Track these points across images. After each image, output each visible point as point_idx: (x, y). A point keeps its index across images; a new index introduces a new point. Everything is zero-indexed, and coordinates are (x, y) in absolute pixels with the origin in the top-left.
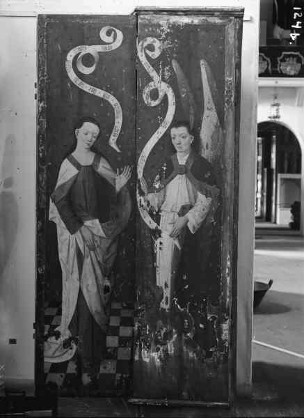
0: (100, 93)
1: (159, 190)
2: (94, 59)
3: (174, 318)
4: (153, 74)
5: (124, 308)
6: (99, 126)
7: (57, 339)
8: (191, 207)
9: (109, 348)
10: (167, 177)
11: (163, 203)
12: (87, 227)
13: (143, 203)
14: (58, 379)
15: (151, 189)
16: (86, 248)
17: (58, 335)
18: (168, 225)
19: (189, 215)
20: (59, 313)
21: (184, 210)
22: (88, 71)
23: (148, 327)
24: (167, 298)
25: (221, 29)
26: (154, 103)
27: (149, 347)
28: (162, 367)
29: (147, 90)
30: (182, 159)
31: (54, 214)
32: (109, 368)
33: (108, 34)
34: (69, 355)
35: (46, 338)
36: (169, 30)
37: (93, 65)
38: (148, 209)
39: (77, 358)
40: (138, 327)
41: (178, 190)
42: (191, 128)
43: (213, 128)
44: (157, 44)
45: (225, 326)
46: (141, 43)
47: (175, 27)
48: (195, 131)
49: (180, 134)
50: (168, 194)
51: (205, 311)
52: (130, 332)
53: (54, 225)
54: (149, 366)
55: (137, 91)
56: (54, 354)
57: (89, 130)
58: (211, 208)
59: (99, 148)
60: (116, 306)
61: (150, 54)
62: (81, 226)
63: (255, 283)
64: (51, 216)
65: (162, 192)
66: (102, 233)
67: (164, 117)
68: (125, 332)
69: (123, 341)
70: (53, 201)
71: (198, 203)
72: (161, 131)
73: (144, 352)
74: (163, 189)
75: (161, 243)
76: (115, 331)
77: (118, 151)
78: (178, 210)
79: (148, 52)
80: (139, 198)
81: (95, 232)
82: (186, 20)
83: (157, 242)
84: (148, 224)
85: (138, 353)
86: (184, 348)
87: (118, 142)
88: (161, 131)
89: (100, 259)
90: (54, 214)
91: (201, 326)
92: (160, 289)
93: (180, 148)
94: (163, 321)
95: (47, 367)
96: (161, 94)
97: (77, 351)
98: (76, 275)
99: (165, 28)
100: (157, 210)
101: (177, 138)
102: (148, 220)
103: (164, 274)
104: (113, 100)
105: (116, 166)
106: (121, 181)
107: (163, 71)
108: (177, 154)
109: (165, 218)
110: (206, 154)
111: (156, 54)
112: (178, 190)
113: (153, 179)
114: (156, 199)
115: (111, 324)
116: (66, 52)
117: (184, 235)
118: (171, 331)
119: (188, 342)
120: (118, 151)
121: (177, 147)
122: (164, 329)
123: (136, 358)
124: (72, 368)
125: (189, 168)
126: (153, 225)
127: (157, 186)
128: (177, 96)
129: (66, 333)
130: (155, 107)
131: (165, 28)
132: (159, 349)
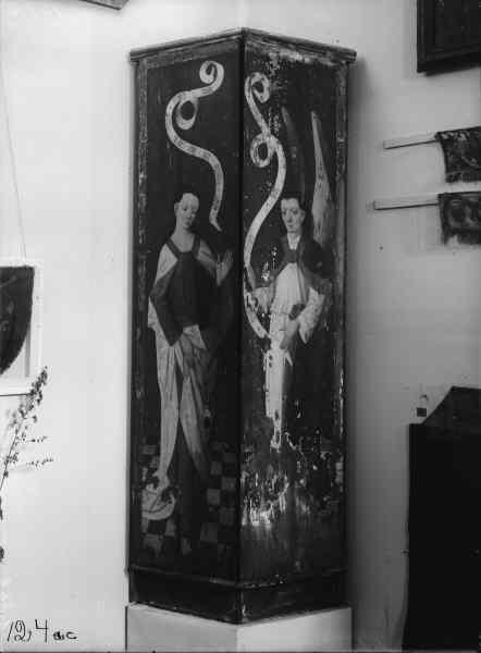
0: (200, 152)
1: (268, 284)
2: (193, 109)
3: (287, 460)
4: (262, 123)
5: (227, 451)
6: (199, 197)
7: (155, 487)
8: (303, 307)
9: (210, 505)
10: (278, 266)
11: (272, 301)
12: (186, 335)
13: (252, 302)
14: (154, 541)
15: (260, 283)
16: (187, 367)
17: (156, 482)
18: (278, 333)
19: (301, 318)
20: (158, 453)
21: (297, 310)
22: (186, 125)
23: (257, 476)
24: (278, 433)
25: (332, 72)
26: (264, 164)
27: (258, 505)
28: (274, 531)
29: (255, 145)
30: (293, 242)
31: (153, 319)
32: (209, 535)
33: (208, 72)
34: (166, 513)
35: (143, 485)
36: (278, 67)
37: (191, 118)
38: (256, 309)
39: (176, 516)
40: (246, 478)
41: (289, 283)
42: (302, 201)
43: (325, 203)
44: (266, 84)
45: (339, 466)
46: (248, 79)
47: (284, 62)
48: (306, 207)
49: (290, 204)
50: (278, 288)
51: (319, 447)
52: (232, 486)
53: (151, 333)
54: (258, 531)
55: (242, 146)
56: (152, 507)
57: (189, 200)
58: (323, 309)
59: (199, 227)
60: (217, 447)
61: (258, 95)
62: (179, 335)
63: (451, 180)
64: (150, 321)
65: (272, 285)
66: (202, 344)
67: (274, 184)
68: (228, 484)
69: (225, 497)
70: (153, 301)
71: (311, 301)
72: (270, 202)
73: (253, 512)
74: (272, 282)
75: (271, 358)
76: (217, 486)
77: (219, 229)
78: (290, 310)
79: (256, 92)
80: (246, 294)
81: (195, 342)
82: (297, 56)
83: (266, 356)
84: (256, 330)
85: (245, 515)
86: (297, 500)
87: (218, 219)
88: (270, 202)
89: (200, 377)
90: (153, 319)
91: (315, 468)
92: (270, 421)
93: (291, 226)
94: (273, 465)
95: (145, 524)
96: (270, 152)
97: (177, 504)
98: (174, 403)
99: (274, 63)
100: (266, 310)
101: (288, 212)
102: (256, 325)
103: (274, 403)
104: (213, 161)
105: (217, 252)
106: (222, 270)
107: (273, 121)
108: (289, 235)
109: (278, 321)
110: (318, 236)
111: (265, 96)
112: (289, 283)
113: (262, 267)
114: (265, 296)
115: (212, 472)
116: (165, 104)
117: (297, 347)
118: (283, 479)
119: (303, 493)
120: (219, 229)
121: (287, 225)
122: (275, 477)
123: (244, 523)
124: (170, 529)
125: (301, 253)
126: (261, 333)
127: (266, 278)
128: (286, 150)
129: (165, 483)
130: (264, 168)
131: (274, 63)
132: (269, 506)
